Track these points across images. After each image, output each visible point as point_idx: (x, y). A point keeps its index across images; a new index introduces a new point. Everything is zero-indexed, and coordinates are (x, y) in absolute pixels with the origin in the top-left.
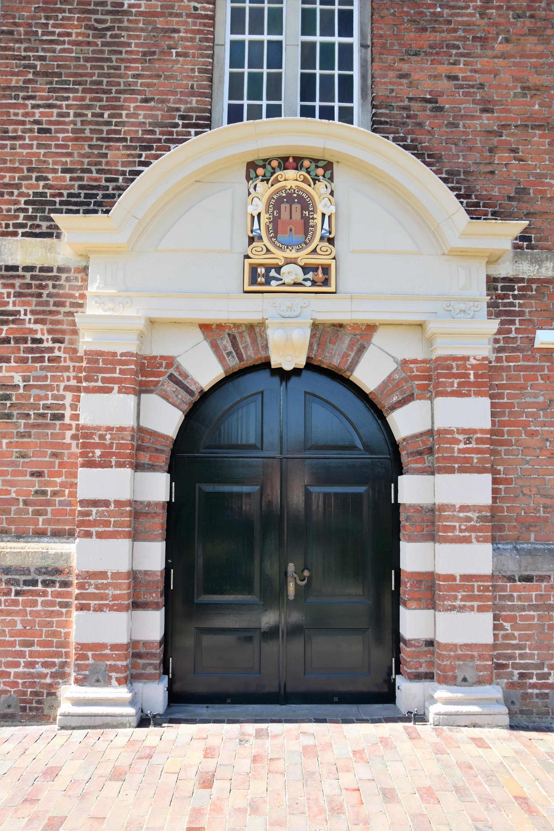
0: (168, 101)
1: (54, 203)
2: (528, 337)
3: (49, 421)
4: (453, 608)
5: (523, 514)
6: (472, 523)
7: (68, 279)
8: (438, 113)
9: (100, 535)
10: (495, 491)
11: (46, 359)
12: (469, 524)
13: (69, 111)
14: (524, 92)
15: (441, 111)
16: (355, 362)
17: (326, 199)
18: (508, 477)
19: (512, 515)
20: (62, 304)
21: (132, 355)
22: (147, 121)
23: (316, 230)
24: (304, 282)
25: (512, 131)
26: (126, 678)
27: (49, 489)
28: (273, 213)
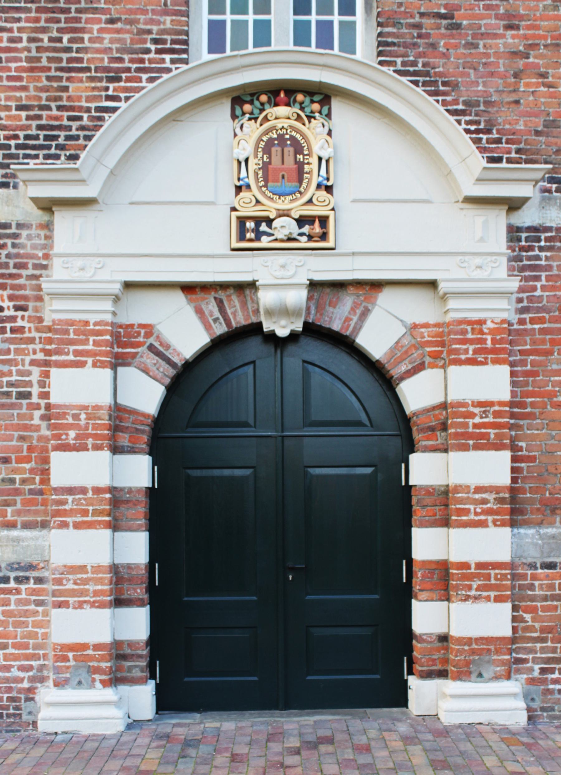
0: (137, 21)
1: (9, 147)
2: (555, 295)
3: (14, 400)
4: (467, 598)
5: (547, 495)
6: (489, 505)
7: (29, 237)
8: (454, 31)
9: (77, 526)
10: (514, 470)
11: (8, 329)
12: (485, 506)
13: (21, 35)
14: (555, 4)
15: (457, 29)
16: (358, 327)
17: (323, 140)
18: (531, 454)
19: (536, 496)
20: (23, 266)
21: (107, 324)
22: (114, 46)
23: (311, 177)
24: (299, 238)
25: (541, 51)
26: (111, 679)
27: (18, 477)
28: (262, 158)
